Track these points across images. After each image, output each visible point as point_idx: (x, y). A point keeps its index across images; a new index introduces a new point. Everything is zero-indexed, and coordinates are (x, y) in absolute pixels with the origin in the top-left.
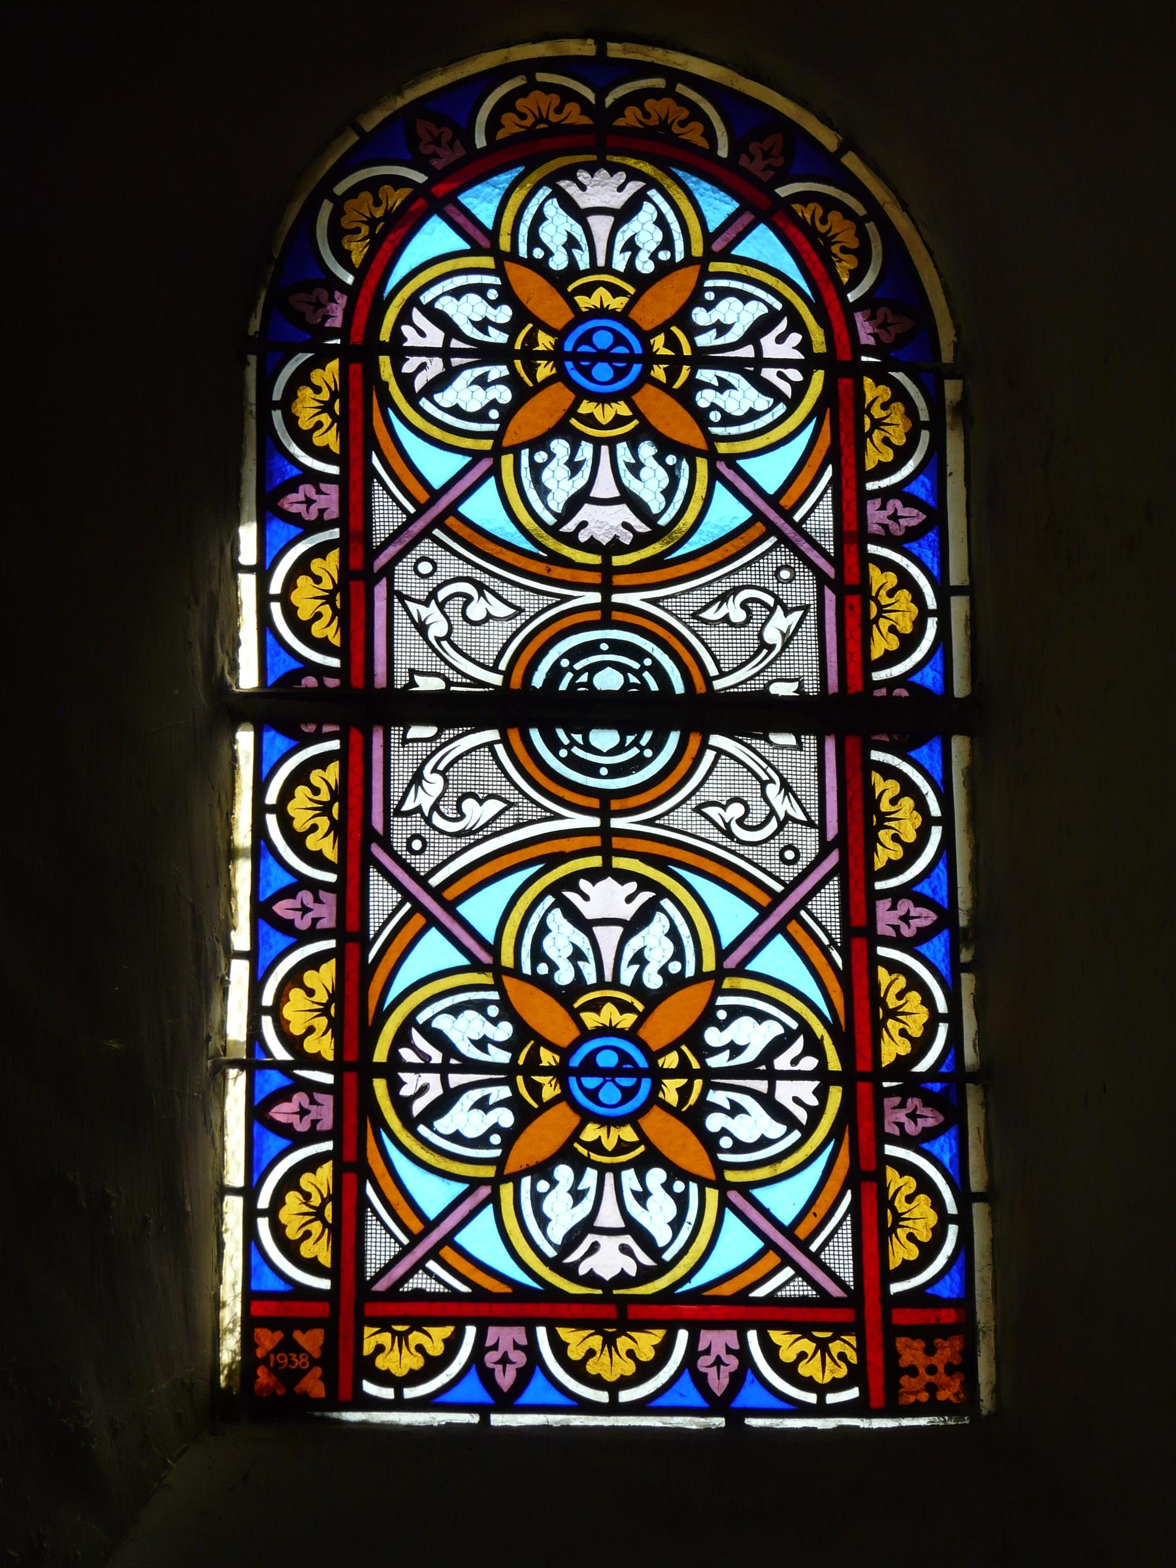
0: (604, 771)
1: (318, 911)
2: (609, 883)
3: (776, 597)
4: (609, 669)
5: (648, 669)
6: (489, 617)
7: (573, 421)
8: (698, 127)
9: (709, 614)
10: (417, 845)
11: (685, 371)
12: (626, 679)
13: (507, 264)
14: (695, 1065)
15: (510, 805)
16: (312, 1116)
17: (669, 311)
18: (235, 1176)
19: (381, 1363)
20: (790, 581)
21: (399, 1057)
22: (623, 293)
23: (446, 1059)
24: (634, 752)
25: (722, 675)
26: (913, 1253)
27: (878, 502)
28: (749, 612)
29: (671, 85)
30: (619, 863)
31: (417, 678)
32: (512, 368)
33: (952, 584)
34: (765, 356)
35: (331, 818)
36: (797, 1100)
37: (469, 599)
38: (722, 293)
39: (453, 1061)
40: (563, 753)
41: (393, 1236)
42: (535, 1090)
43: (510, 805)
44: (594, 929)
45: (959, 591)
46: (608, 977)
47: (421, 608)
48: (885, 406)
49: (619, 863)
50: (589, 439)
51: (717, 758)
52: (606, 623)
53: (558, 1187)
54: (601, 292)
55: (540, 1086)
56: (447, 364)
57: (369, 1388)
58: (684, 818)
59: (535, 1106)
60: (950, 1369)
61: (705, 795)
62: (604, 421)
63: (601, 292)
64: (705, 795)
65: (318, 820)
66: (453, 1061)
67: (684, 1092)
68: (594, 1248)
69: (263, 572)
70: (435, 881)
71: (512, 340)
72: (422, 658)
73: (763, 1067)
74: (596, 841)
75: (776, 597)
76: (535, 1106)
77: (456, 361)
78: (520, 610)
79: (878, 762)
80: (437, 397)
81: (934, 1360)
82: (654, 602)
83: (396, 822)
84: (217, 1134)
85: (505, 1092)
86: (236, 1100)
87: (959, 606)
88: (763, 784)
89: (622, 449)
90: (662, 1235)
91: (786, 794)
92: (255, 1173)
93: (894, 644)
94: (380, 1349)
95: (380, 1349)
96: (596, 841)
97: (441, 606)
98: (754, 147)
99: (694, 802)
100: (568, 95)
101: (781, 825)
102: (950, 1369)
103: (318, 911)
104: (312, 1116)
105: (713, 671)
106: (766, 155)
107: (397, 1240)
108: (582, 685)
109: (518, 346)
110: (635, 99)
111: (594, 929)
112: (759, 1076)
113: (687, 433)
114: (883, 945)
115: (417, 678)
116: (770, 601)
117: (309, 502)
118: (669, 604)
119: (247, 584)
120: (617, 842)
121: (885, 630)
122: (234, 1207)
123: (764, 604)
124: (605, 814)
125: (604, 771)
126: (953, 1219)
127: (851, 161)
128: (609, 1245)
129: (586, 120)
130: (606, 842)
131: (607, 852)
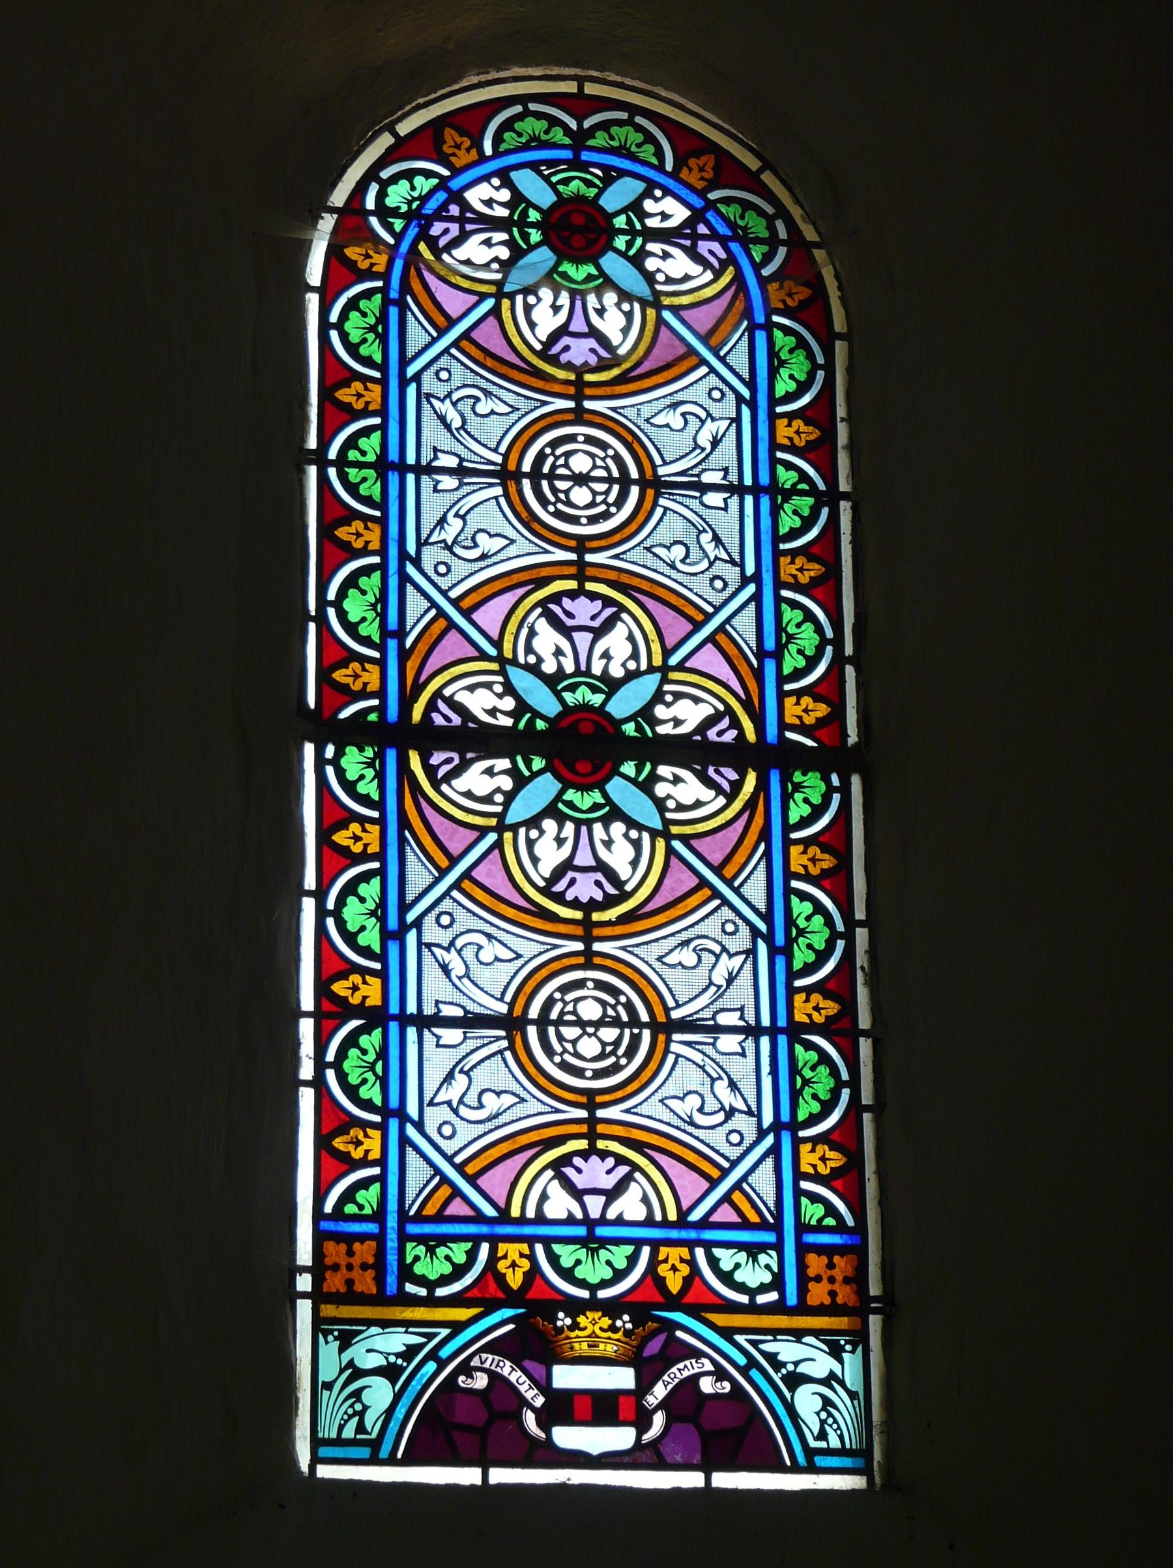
0: (581, 438)
1: (368, 536)
2: (578, 362)
3: (707, 412)
4: (581, 505)
5: (623, 1005)
6: (492, 412)
7: (560, 806)
8: (650, 148)
9: (656, 421)
10: (442, 569)
11: (639, 241)
12: (605, 1011)
13: (508, 667)
14: (638, 226)
15: (512, 541)
16: (364, 1147)
17: (638, 705)
18: (310, 882)
19: (418, 1269)
20: (719, 401)
21: (431, 718)
22: (593, 185)
23: (462, 212)
24: (613, 1059)
25: (678, 1006)
26: (801, 663)
27: (785, 421)
28: (699, 958)
29: (631, 117)
30: (590, 586)
31: (441, 1006)
32: (514, 762)
33: (841, 489)
34: (726, 1204)
35: (375, 769)
36: (710, 252)
37: (477, 399)
38: (678, 696)
39: (469, 215)
40: (557, 1059)
41: (427, 331)
42: (525, 237)
43: (512, 541)
44: (574, 634)
45: (861, 924)
46: (584, 829)
47: (444, 953)
48: (813, 1068)
49: (590, 586)
50: (572, 819)
51: (664, 514)
52: (588, 965)
53: (545, 836)
54: (583, 689)
55: (529, 234)
56: (462, 229)
57: (410, 1288)
58: (639, 555)
59: (525, 247)
60: (846, 1280)
61: (656, 538)
62: (583, 688)
63: (583, 689)
64: (656, 538)
65: (365, 772)
66: (469, 215)
67: (629, 244)
68: (572, 882)
69: (320, 895)
70: (458, 1160)
71: (516, 723)
72: (448, 993)
73: (698, 738)
74: (584, 1129)
75: (707, 412)
76: (525, 247)
77: (469, 227)
78: (515, 409)
79: (776, 253)
80: (454, 252)
81: (834, 1272)
82: (616, 557)
83: (428, 1111)
84: (291, 1337)
85: (504, 236)
86: (305, 1243)
87: (862, 934)
88: (713, 1080)
89: (598, 828)
90: (624, 872)
91: (716, 546)
92: (325, 440)
93: (811, 957)
94: (417, 1259)
95: (417, 1259)
96: (584, 1129)
97: (459, 952)
98: (692, 162)
99: (659, 1096)
100: (553, 122)
101: (711, 564)
102: (846, 1280)
103: (368, 536)
104: (364, 1147)
105: (671, 1003)
106: (701, 169)
107: (430, 334)
108: (569, 1013)
109: (516, 218)
110: (605, 126)
111: (574, 634)
112: (686, 237)
113: (638, 286)
114: (784, 588)
115: (440, 455)
116: (703, 415)
117: (355, 988)
118: (628, 556)
119: (309, 905)
120: (600, 1129)
121: (794, 654)
122: (309, 905)
123: (697, 416)
124: (591, 1106)
125: (581, 438)
126: (821, 367)
127: (767, 178)
128: (582, 619)
129: (567, 141)
130: (579, 390)
131: (581, 578)
